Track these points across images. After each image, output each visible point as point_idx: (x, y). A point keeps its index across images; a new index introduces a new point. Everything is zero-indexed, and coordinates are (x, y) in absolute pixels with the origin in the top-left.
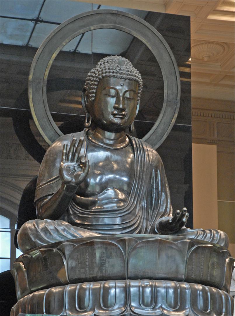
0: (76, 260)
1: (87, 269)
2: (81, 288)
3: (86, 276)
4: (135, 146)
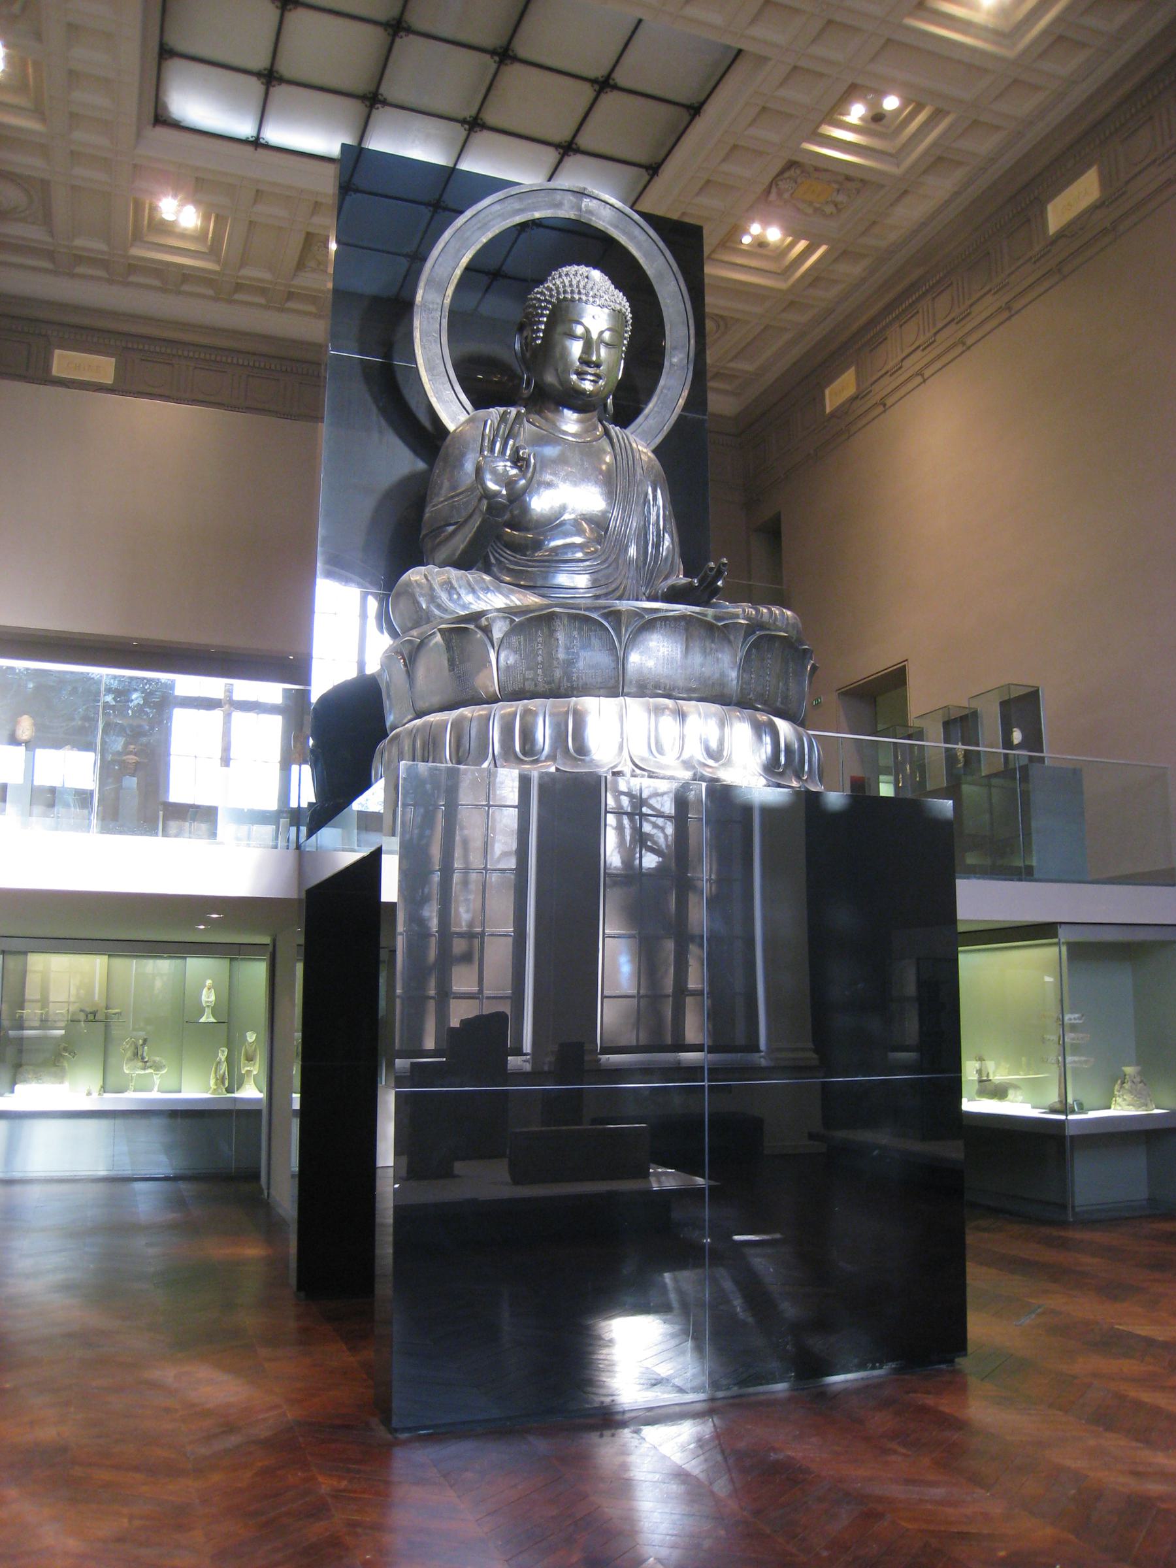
0: (515, 652)
1: (540, 671)
2: (527, 712)
3: (536, 685)
4: (615, 440)
